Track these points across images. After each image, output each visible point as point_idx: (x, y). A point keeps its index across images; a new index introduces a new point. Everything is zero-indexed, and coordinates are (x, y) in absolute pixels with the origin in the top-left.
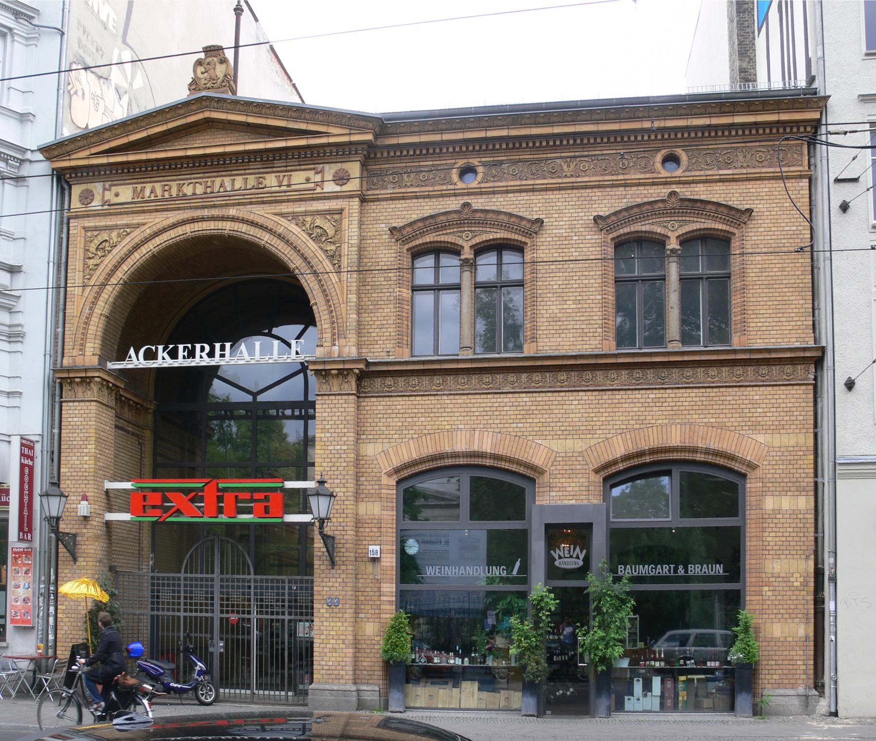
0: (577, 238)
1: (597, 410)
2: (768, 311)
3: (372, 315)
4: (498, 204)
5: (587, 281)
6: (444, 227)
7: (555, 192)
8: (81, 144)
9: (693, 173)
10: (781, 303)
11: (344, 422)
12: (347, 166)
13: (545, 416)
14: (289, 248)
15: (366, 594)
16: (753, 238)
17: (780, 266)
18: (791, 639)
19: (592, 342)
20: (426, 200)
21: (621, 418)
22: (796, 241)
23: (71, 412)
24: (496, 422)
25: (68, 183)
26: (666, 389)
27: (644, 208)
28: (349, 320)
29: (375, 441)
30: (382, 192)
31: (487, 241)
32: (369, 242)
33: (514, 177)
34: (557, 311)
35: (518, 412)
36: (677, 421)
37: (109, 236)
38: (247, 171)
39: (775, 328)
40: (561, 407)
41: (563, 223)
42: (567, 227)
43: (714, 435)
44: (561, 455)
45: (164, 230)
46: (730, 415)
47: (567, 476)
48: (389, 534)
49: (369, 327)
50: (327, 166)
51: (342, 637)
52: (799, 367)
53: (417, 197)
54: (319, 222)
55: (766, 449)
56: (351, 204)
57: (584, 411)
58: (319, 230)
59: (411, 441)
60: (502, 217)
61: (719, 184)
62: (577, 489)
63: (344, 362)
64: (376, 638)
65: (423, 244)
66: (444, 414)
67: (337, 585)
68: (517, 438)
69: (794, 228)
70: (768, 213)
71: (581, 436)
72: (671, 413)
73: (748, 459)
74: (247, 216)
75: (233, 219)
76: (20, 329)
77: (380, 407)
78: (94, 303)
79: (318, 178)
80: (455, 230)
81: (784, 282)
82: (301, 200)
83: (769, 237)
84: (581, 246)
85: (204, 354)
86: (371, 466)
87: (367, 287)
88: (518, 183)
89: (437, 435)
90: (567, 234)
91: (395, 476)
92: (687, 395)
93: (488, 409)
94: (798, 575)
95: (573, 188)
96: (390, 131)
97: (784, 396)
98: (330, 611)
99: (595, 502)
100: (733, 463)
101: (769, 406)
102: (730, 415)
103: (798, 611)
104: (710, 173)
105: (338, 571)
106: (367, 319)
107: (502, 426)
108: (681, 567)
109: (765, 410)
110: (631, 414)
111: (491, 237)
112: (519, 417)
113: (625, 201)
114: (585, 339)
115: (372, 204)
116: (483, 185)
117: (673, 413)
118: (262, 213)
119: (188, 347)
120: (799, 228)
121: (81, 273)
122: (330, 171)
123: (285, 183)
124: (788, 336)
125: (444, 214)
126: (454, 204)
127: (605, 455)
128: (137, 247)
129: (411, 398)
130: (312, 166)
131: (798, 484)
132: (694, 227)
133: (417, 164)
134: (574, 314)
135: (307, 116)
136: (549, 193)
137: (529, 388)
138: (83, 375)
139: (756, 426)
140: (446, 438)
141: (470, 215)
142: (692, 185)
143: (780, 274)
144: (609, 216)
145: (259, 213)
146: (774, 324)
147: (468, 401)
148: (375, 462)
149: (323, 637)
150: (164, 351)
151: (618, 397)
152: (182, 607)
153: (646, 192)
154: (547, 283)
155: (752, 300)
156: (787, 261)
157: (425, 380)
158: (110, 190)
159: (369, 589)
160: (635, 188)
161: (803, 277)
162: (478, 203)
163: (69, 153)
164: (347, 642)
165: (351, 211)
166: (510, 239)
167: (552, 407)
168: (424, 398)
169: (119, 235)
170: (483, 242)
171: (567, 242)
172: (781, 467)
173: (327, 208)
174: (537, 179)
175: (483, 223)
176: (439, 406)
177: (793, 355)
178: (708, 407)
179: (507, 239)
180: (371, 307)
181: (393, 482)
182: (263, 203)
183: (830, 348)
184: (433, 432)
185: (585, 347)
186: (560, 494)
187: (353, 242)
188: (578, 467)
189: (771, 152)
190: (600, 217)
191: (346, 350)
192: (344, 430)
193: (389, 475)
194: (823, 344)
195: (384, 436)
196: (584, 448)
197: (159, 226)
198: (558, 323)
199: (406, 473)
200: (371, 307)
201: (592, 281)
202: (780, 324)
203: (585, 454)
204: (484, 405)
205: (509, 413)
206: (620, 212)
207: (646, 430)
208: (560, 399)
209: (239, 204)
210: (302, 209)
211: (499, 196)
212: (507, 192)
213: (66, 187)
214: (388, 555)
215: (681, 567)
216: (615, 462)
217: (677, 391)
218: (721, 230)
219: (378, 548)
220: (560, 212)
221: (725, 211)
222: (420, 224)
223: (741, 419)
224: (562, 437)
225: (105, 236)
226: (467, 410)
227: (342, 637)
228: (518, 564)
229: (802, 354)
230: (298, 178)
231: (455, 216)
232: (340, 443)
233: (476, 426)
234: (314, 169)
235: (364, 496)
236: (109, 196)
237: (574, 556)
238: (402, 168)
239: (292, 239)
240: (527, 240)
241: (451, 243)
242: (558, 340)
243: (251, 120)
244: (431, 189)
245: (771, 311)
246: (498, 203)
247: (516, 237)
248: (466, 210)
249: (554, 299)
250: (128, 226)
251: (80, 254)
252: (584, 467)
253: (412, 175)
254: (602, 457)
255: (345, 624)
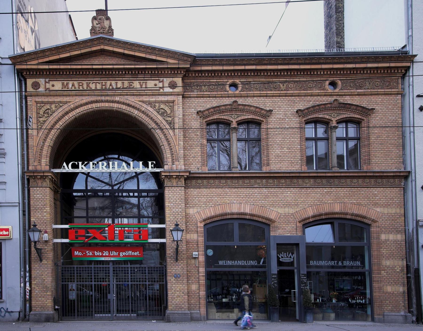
0: (288, 119)
1: (299, 196)
2: (381, 155)
3: (190, 151)
4: (249, 102)
5: (293, 139)
6: (223, 112)
7: (277, 98)
8: (33, 57)
9: (344, 91)
10: (387, 151)
11: (180, 199)
12: (175, 79)
13: (275, 198)
14: (148, 118)
15: (191, 272)
16: (374, 122)
17: (387, 135)
18: (396, 293)
19: (296, 167)
20: (214, 99)
21: (311, 200)
22: (395, 124)
23: (35, 192)
24: (251, 200)
25: (23, 76)
26: (332, 188)
27: (321, 107)
28: (180, 153)
29: (193, 207)
30: (191, 93)
31: (244, 119)
32: (186, 117)
33: (257, 89)
34: (279, 152)
35: (262, 196)
36: (338, 201)
37: (50, 107)
38: (124, 79)
39: (384, 163)
40: (282, 194)
41: (281, 112)
42: (283, 114)
43: (355, 207)
44: (283, 215)
45: (81, 105)
46: (363, 200)
47: (286, 224)
48: (201, 247)
49: (188, 157)
50: (165, 79)
51: (182, 291)
52: (397, 180)
53: (209, 97)
54: (162, 106)
55: (381, 214)
56: (178, 98)
57: (293, 196)
58: (162, 110)
59: (211, 208)
60: (252, 108)
61: (357, 96)
62: (291, 229)
63: (179, 172)
64: (197, 291)
65: (213, 119)
66: (226, 196)
67: (179, 269)
68: (262, 207)
69: (394, 118)
70: (381, 111)
71: (292, 207)
72: (335, 198)
73: (373, 218)
74: (126, 101)
75: (118, 102)
76: (3, 151)
77: (195, 193)
78: (45, 140)
79: (161, 85)
80: (229, 113)
81: (389, 142)
82: (153, 95)
83: (381, 122)
84: (290, 123)
85: (104, 167)
86: (192, 218)
87: (187, 139)
88: (259, 92)
89: (223, 205)
90: (283, 118)
91: (203, 223)
92: (342, 190)
93: (248, 194)
94: (399, 267)
95: (286, 96)
96: (198, 63)
97: (389, 192)
98: (176, 280)
99: (300, 234)
100: (365, 220)
101: (382, 196)
102: (363, 200)
103: (399, 281)
104: (352, 91)
105: (179, 263)
106: (187, 153)
107: (254, 202)
108: (340, 262)
109: (380, 198)
110: (316, 198)
111: (246, 118)
112: (262, 198)
113: (311, 103)
114: (293, 165)
115: (187, 99)
116: (242, 93)
117: (336, 198)
118: (133, 100)
119: (154, 163)
120: (396, 118)
121: (36, 125)
122: (167, 81)
123: (144, 86)
124: (391, 166)
125: (224, 106)
126: (228, 101)
127: (304, 215)
128: (67, 113)
129: (210, 189)
130: (158, 78)
131: (397, 229)
132: (345, 116)
133: (209, 81)
134: (287, 154)
135: (157, 52)
136: (274, 98)
137: (267, 186)
138: (42, 174)
139: (376, 205)
140: (228, 207)
141: (237, 107)
142: (344, 97)
143: (387, 138)
144: (304, 110)
145: (131, 100)
146: (384, 161)
147: (238, 191)
148: (194, 216)
149: (172, 291)
150: (82, 165)
151: (309, 191)
152: (93, 280)
153: (321, 99)
154: (274, 140)
155: (373, 150)
156: (390, 133)
157: (217, 181)
158: (49, 83)
159: (193, 271)
160: (316, 97)
161: (398, 140)
162: (240, 101)
163: (26, 61)
164: (185, 293)
165: (179, 102)
166: (255, 119)
167: (278, 194)
168: (216, 189)
169: (56, 107)
170: (242, 120)
171: (283, 121)
172: (388, 222)
173: (166, 99)
174: (268, 91)
175: (242, 111)
176: (224, 193)
177: (394, 174)
178: (352, 196)
179: (254, 119)
180: (189, 148)
181: (202, 225)
182: (133, 95)
183: (413, 172)
184: (221, 204)
185: (293, 168)
186: (283, 231)
187: (180, 117)
188: (291, 220)
189: (383, 82)
190: (300, 110)
191: (179, 166)
192: (180, 203)
193: (201, 222)
194: (409, 169)
195: (197, 205)
196: (294, 212)
197: (78, 104)
198: (280, 158)
199: (208, 221)
200: (189, 148)
201: (295, 139)
202: (387, 161)
203: (294, 214)
204: (246, 193)
205: (257, 196)
206: (309, 108)
207: (323, 205)
208: (282, 191)
209: (121, 95)
210: (154, 99)
211: (250, 98)
212: (254, 96)
213: (22, 79)
214: (202, 256)
215: (340, 262)
216: (309, 218)
217: (337, 189)
218: (357, 118)
219: (197, 253)
220: (279, 107)
221: (361, 109)
222: (212, 110)
223: (368, 201)
224: (283, 207)
225: (48, 106)
226: (237, 194)
227: (182, 291)
228: (262, 260)
229: (399, 174)
230: (151, 84)
231: (229, 107)
232: (178, 208)
233: (242, 202)
234: (158, 80)
235: (189, 231)
236: (48, 86)
237: (289, 257)
238: (201, 82)
239: (150, 114)
240: (264, 120)
241: (226, 120)
242: (280, 165)
243: (126, 52)
244: (216, 93)
245: (382, 155)
246: (249, 101)
247: (258, 118)
248: (235, 104)
249: (278, 147)
250: (61, 102)
251: (34, 115)
252: (294, 220)
253: (207, 87)
254: (302, 216)
255: (184, 285)
